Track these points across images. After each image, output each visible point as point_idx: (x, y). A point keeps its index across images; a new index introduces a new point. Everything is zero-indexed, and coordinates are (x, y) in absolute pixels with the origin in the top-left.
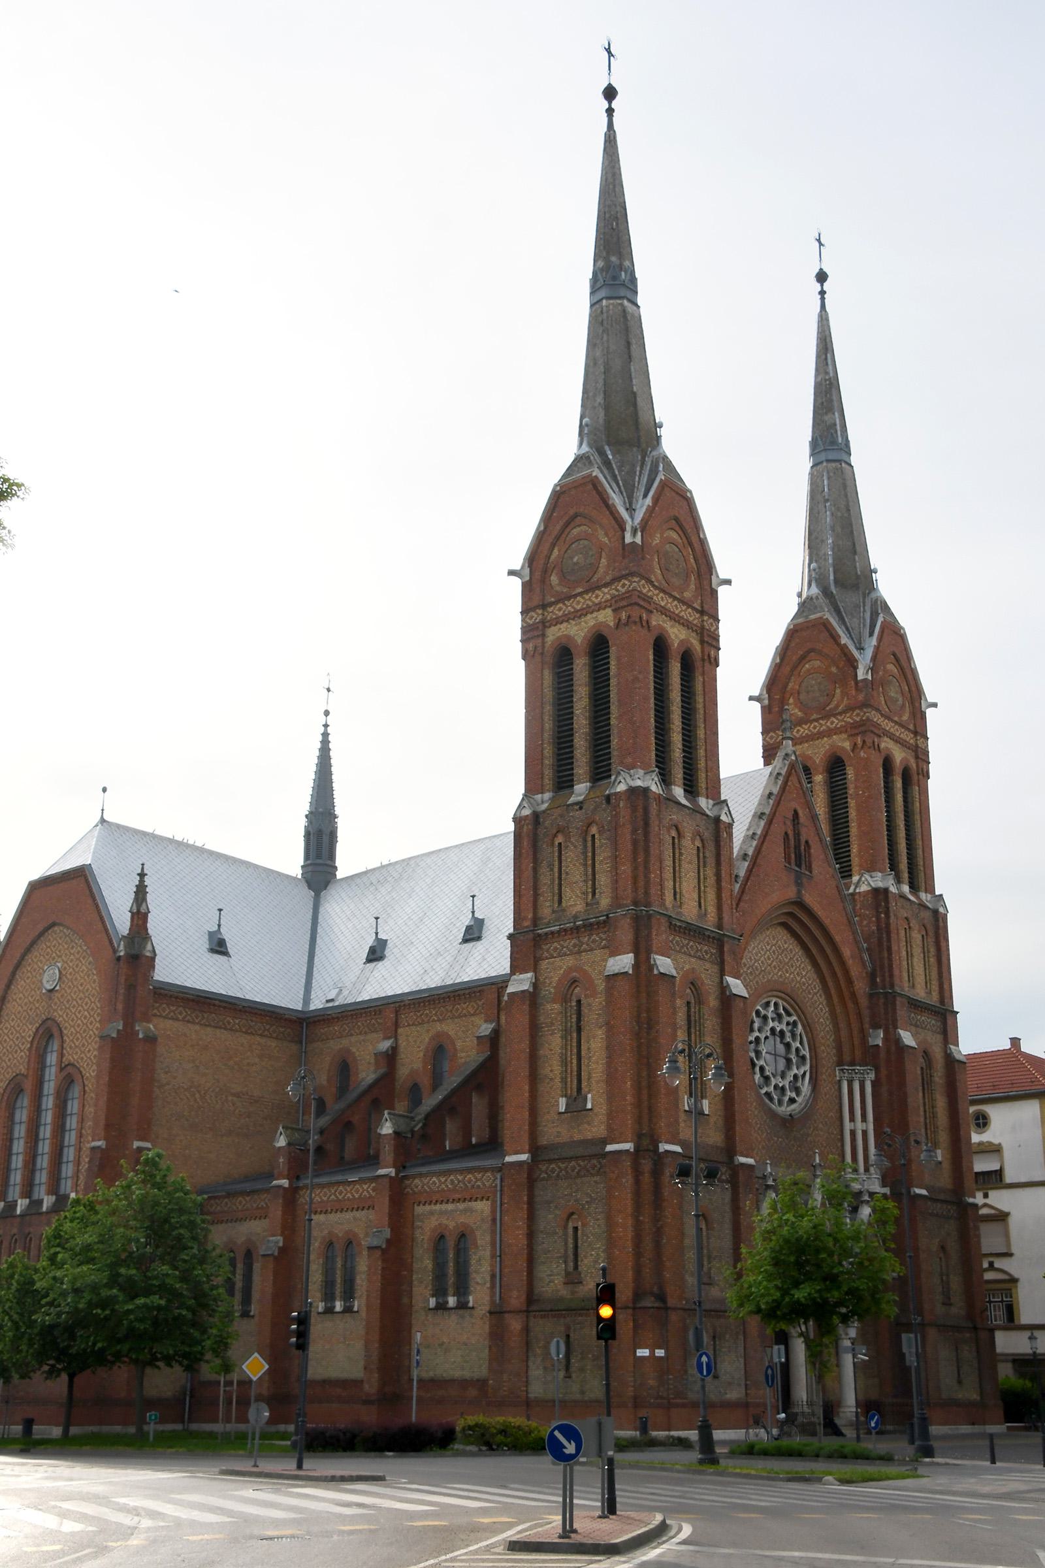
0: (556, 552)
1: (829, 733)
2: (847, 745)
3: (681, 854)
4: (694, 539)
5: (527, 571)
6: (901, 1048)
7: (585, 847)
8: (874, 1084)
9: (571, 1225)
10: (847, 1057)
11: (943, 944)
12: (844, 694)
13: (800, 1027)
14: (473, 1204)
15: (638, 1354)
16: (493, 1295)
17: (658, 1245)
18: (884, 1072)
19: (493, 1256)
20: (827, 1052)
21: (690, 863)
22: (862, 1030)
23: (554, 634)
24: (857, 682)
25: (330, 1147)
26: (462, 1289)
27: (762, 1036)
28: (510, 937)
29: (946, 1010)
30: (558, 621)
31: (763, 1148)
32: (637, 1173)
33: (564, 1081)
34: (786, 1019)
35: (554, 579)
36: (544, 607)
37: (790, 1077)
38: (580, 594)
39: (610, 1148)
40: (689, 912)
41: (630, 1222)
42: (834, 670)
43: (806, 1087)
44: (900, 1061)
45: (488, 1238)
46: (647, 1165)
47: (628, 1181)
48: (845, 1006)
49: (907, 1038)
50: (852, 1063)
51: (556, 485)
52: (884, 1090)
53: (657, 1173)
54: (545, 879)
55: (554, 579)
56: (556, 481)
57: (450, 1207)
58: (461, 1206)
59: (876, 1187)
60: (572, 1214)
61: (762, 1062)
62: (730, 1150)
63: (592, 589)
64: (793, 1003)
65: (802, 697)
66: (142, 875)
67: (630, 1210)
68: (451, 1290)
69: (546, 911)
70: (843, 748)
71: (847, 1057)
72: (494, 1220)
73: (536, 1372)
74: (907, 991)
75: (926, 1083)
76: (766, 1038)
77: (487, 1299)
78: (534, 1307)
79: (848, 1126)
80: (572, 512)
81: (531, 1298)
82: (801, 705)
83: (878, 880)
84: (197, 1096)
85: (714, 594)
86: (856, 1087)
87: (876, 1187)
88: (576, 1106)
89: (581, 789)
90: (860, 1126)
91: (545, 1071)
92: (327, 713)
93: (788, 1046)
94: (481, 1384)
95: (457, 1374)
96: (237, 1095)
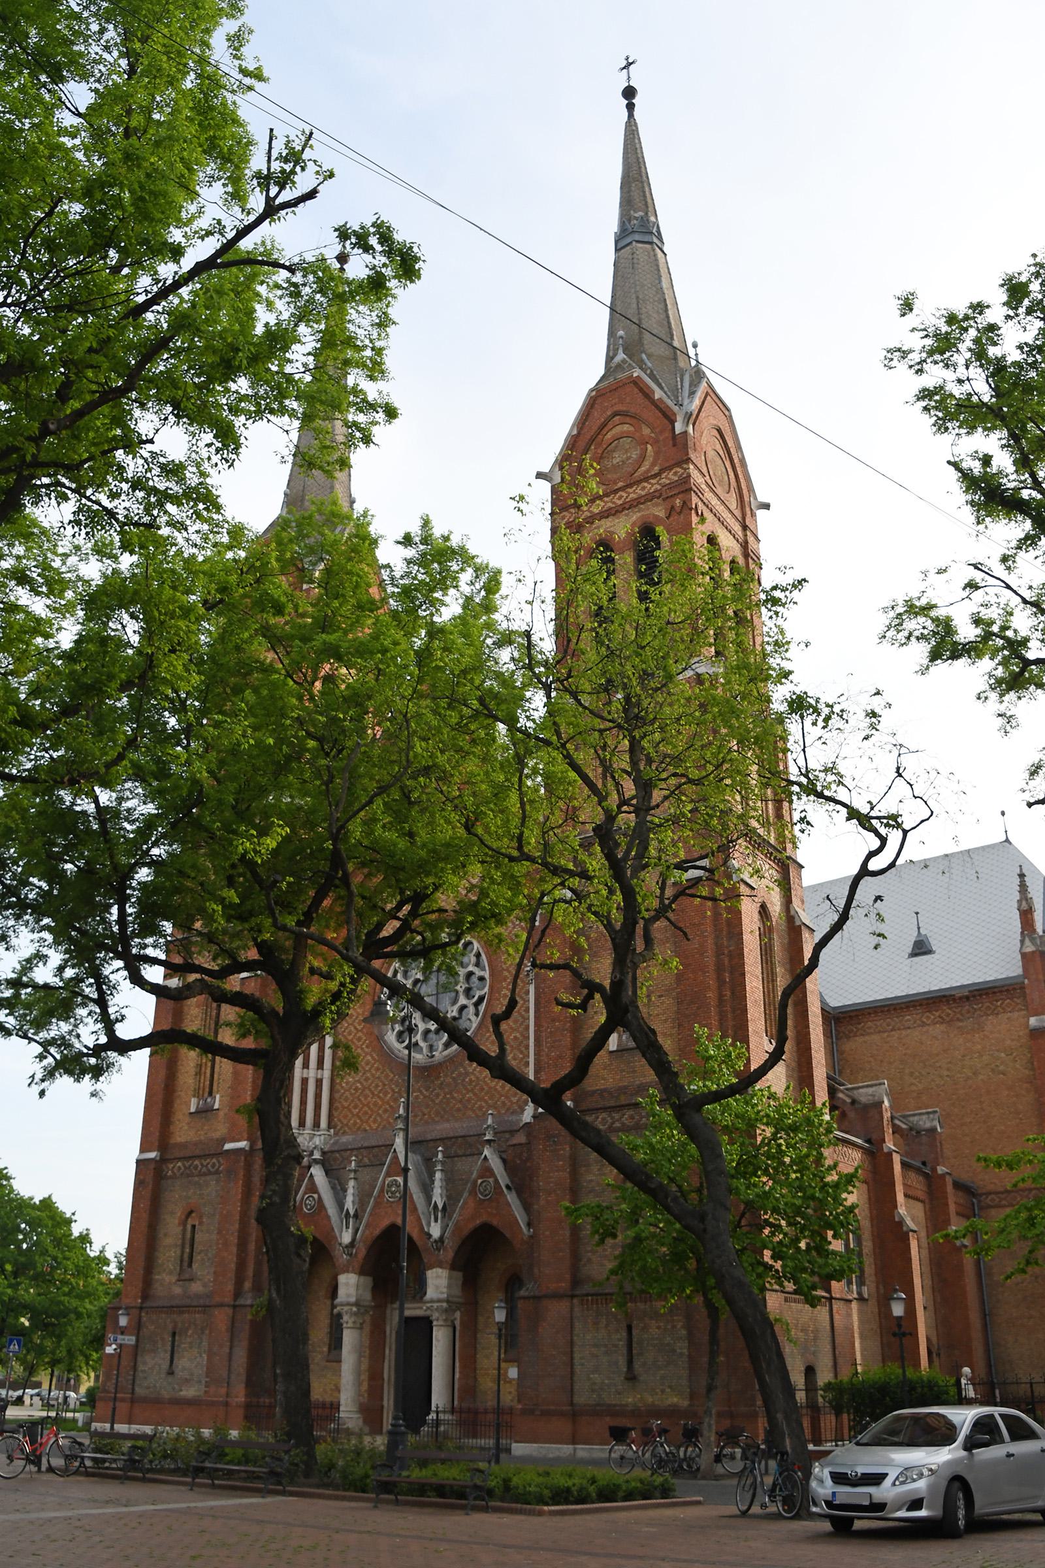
9: (190, 1222)
15: (134, 1338)
29: (789, 858)
31: (386, 1111)
39: (228, 1146)
51: (592, 390)
56: (592, 384)
60: (191, 1212)
78: (148, 1304)
79: (327, 1074)
90: (312, 1073)
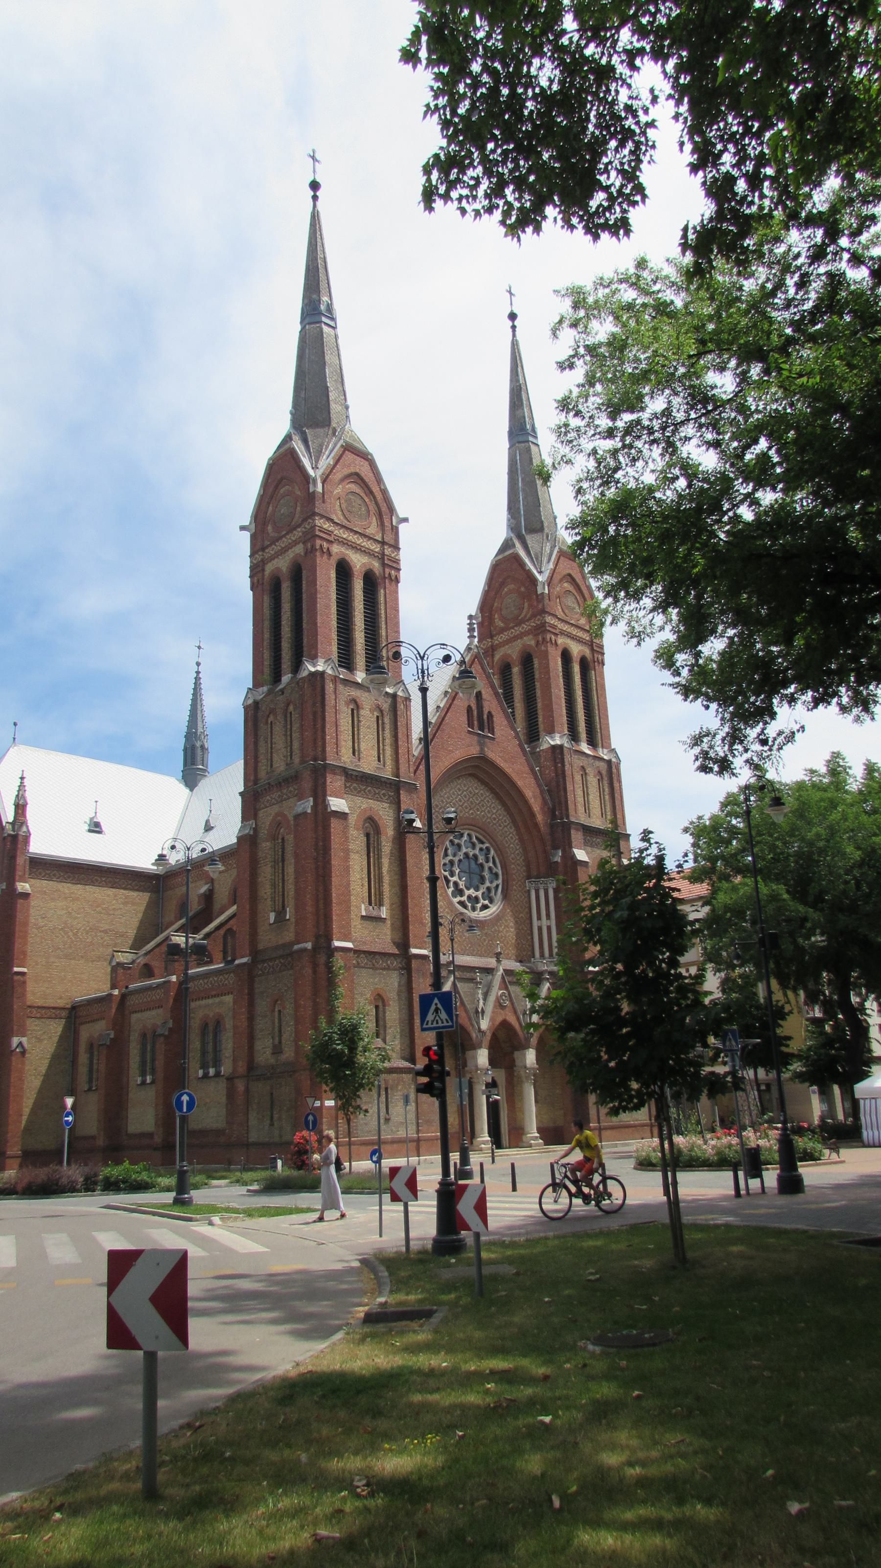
0: (271, 508)
1: (520, 636)
2: (533, 643)
3: (359, 721)
4: (375, 489)
5: (253, 526)
7: (286, 721)
8: (556, 891)
11: (616, 785)
12: (530, 606)
13: (492, 852)
20: (517, 869)
21: (368, 727)
22: (545, 851)
23: (269, 568)
24: (537, 596)
26: (217, 1063)
27: (456, 859)
28: (241, 793)
30: (272, 558)
32: (315, 966)
33: (273, 899)
34: (478, 846)
35: (270, 528)
36: (263, 549)
37: (483, 889)
38: (284, 536)
40: (368, 765)
42: (523, 589)
47: (308, 971)
49: (581, 854)
50: (538, 877)
51: (270, 459)
54: (262, 750)
55: (270, 528)
57: (210, 1001)
58: (217, 1000)
61: (455, 879)
63: (290, 531)
64: (485, 833)
65: (504, 612)
66: (22, 778)
69: (262, 774)
70: (530, 646)
73: (253, 1121)
74: (583, 819)
76: (460, 861)
79: (535, 923)
80: (279, 477)
81: (251, 1066)
82: (503, 619)
83: (557, 740)
84: (70, 934)
85: (395, 531)
89: (286, 678)
92: (198, 664)
93: (482, 865)
94: (219, 1132)
96: (105, 932)
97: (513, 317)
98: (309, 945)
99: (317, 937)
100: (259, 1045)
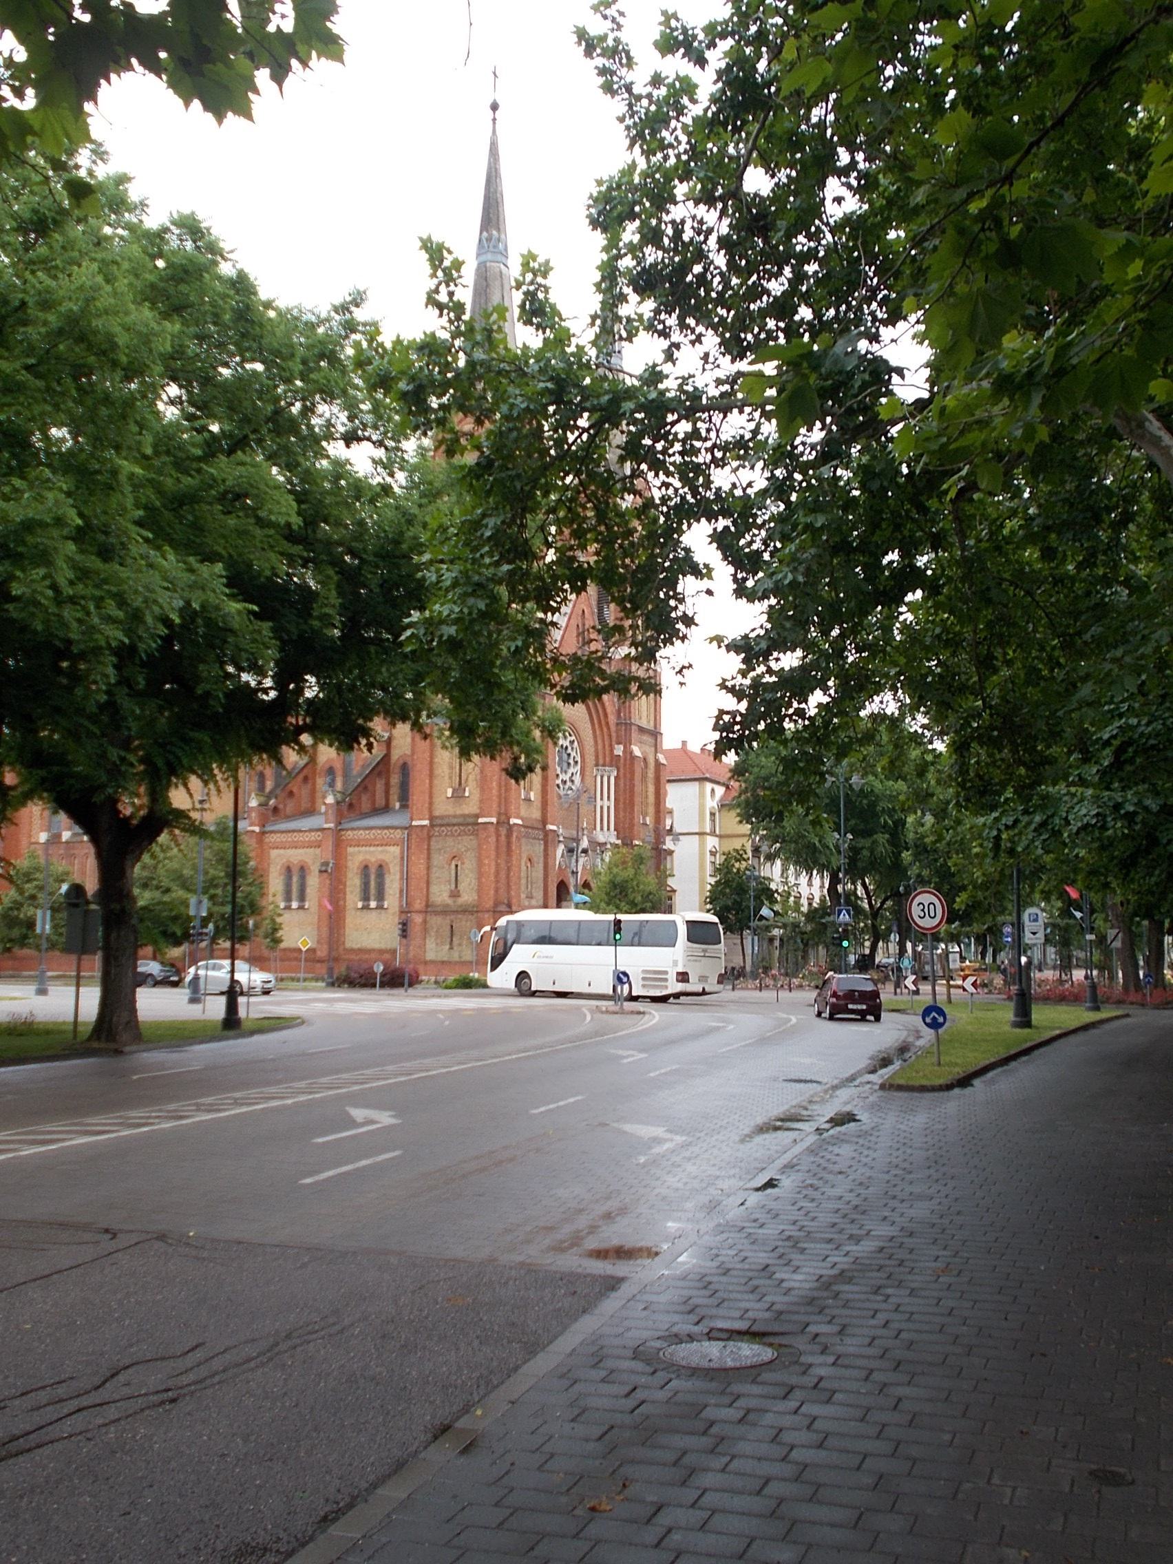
6: (633, 758)
10: (601, 762)
14: (388, 848)
16: (401, 901)
17: (508, 877)
18: (622, 771)
19: (402, 878)
20: (590, 760)
25: (281, 806)
26: (380, 897)
32: (498, 835)
33: (450, 778)
39: (480, 820)
41: (493, 863)
43: (577, 779)
44: (632, 764)
45: (398, 868)
46: (503, 831)
47: (493, 839)
48: (602, 730)
49: (637, 751)
50: (604, 765)
52: (622, 782)
53: (509, 835)
57: (372, 849)
58: (380, 849)
59: (613, 840)
62: (544, 822)
67: (493, 857)
68: (372, 898)
71: (601, 762)
72: (402, 858)
74: (638, 722)
75: (644, 777)
77: (397, 904)
86: (605, 779)
87: (613, 840)
88: (458, 794)
91: (438, 771)
95: (377, 946)
97: (495, 107)
98: (494, 820)
99: (499, 814)
100: (434, 889)
